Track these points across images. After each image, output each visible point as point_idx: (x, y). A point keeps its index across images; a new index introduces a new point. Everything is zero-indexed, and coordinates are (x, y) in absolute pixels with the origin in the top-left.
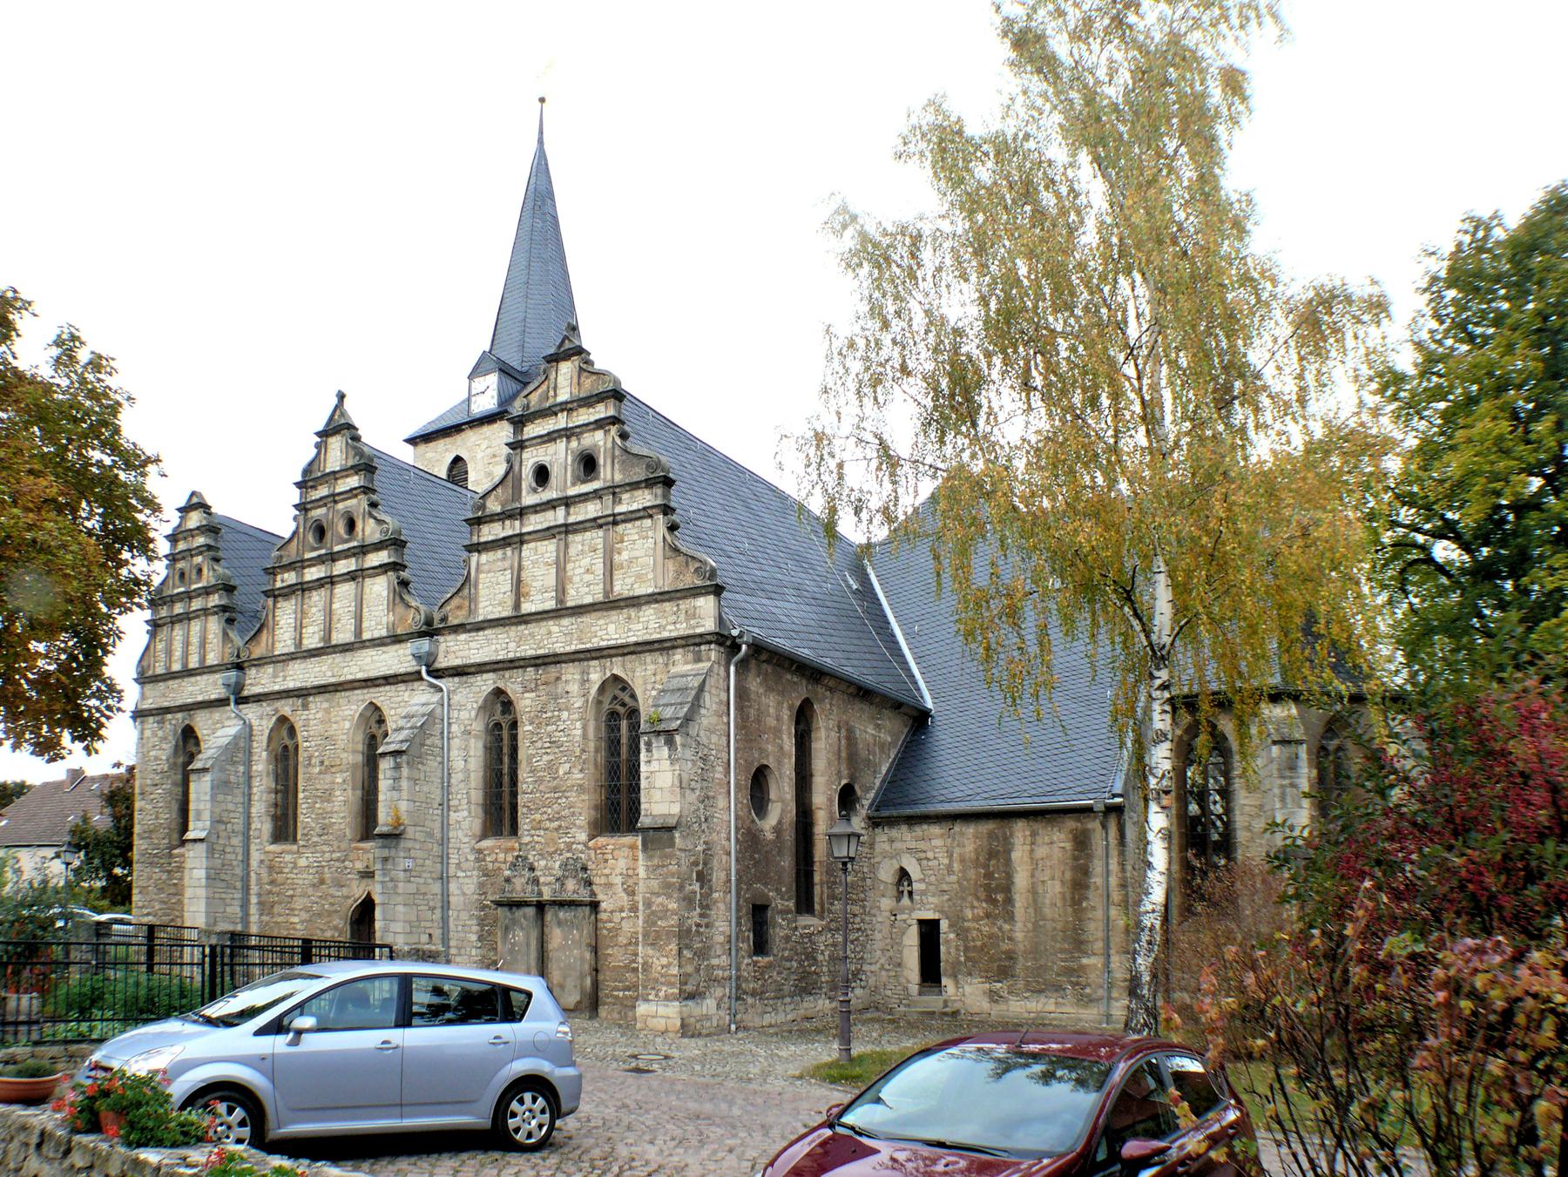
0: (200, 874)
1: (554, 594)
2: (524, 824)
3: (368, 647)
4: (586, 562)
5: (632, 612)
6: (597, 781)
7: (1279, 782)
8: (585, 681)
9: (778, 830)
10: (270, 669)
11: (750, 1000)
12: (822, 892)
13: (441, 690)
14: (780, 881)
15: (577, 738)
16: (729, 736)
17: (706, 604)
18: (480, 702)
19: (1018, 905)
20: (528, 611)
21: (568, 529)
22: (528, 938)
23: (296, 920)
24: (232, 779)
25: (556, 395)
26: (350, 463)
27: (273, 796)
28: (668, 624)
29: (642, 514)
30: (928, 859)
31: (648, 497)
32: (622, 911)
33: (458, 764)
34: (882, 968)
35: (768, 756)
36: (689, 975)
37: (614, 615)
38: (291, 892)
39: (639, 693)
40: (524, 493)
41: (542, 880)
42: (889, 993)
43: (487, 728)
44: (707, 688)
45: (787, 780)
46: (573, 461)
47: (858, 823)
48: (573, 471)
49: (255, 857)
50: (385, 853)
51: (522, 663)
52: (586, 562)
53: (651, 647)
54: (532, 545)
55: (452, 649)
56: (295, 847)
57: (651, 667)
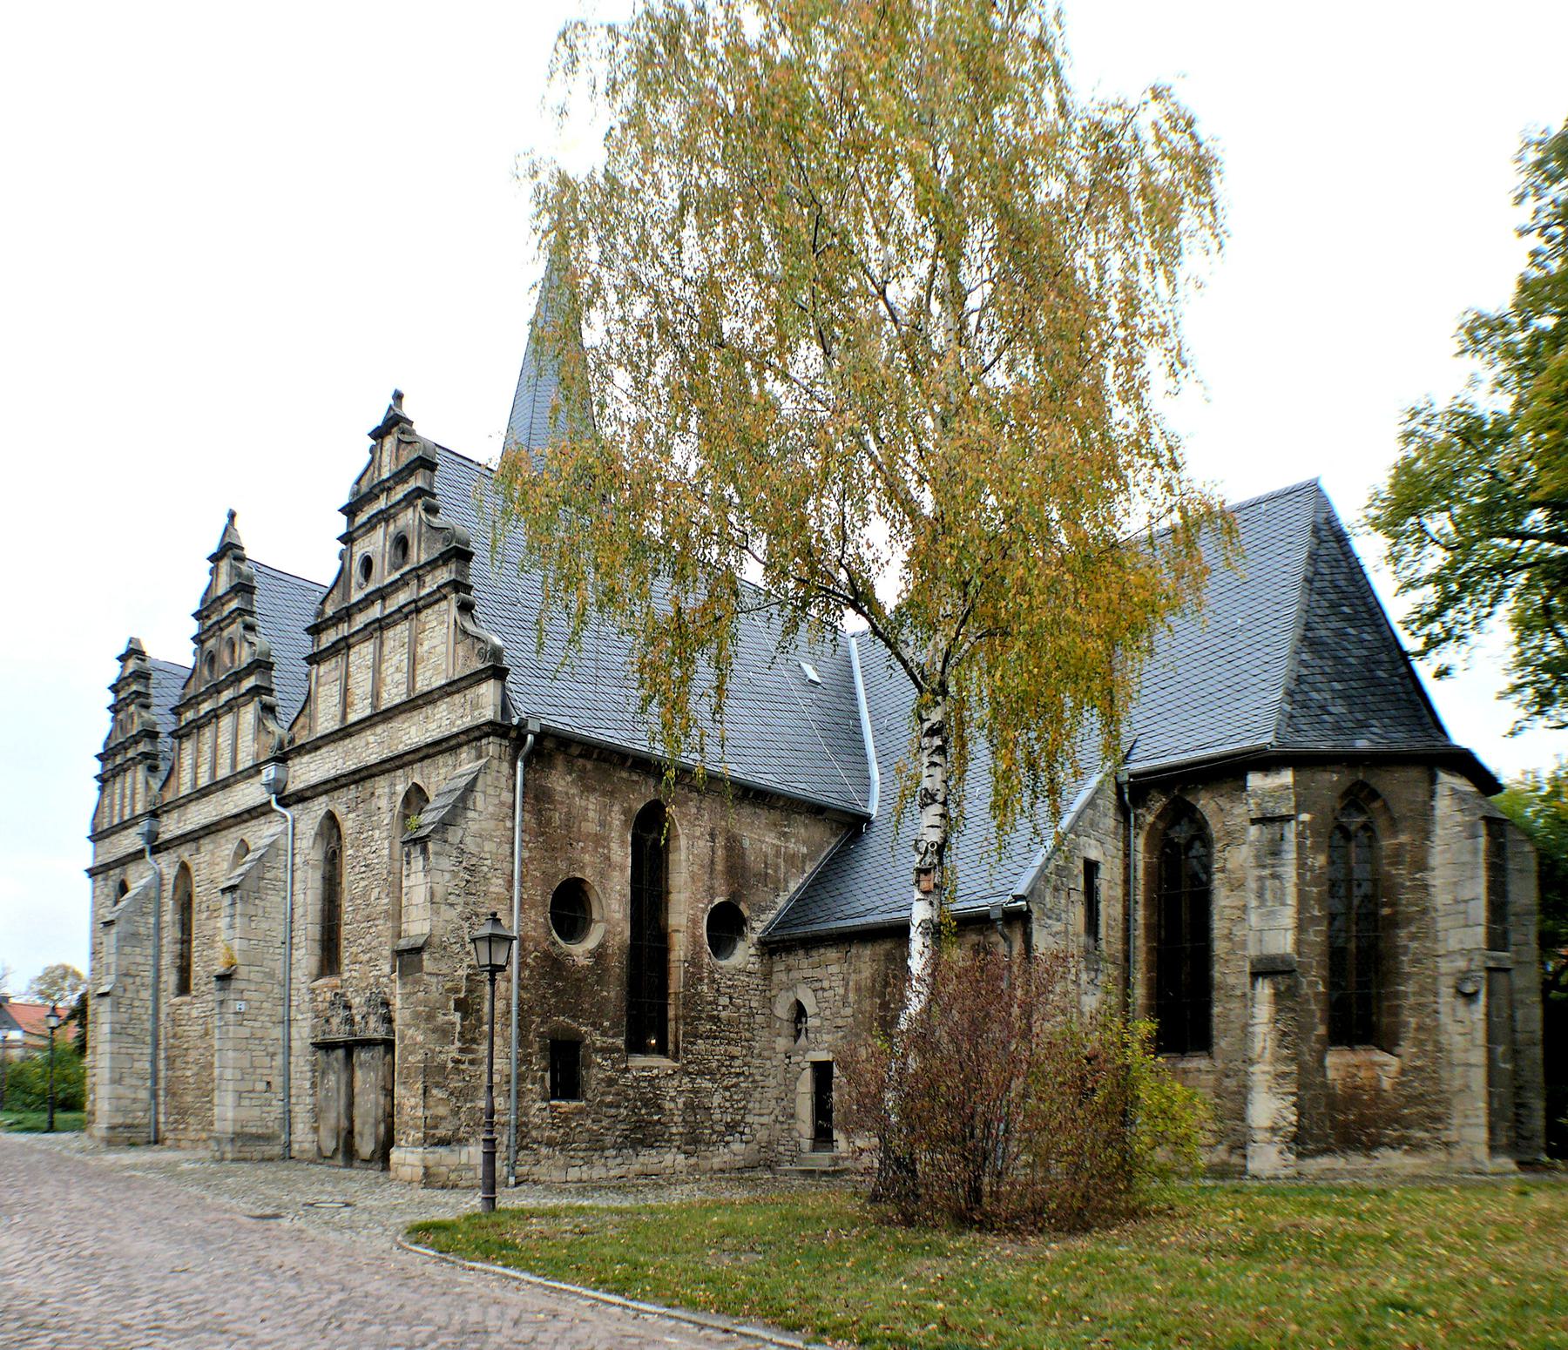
0: (106, 1028)
5: (429, 710)
7: (1257, 872)
9: (599, 954)
10: (175, 815)
11: (544, 1151)
12: (677, 1029)
14: (601, 1013)
17: (488, 691)
22: (338, 1082)
23: (189, 1073)
24: (142, 930)
30: (823, 989)
33: (299, 898)
34: (776, 1121)
35: (582, 868)
36: (442, 1118)
42: (781, 1149)
44: (480, 785)
47: (743, 955)
49: (164, 1009)
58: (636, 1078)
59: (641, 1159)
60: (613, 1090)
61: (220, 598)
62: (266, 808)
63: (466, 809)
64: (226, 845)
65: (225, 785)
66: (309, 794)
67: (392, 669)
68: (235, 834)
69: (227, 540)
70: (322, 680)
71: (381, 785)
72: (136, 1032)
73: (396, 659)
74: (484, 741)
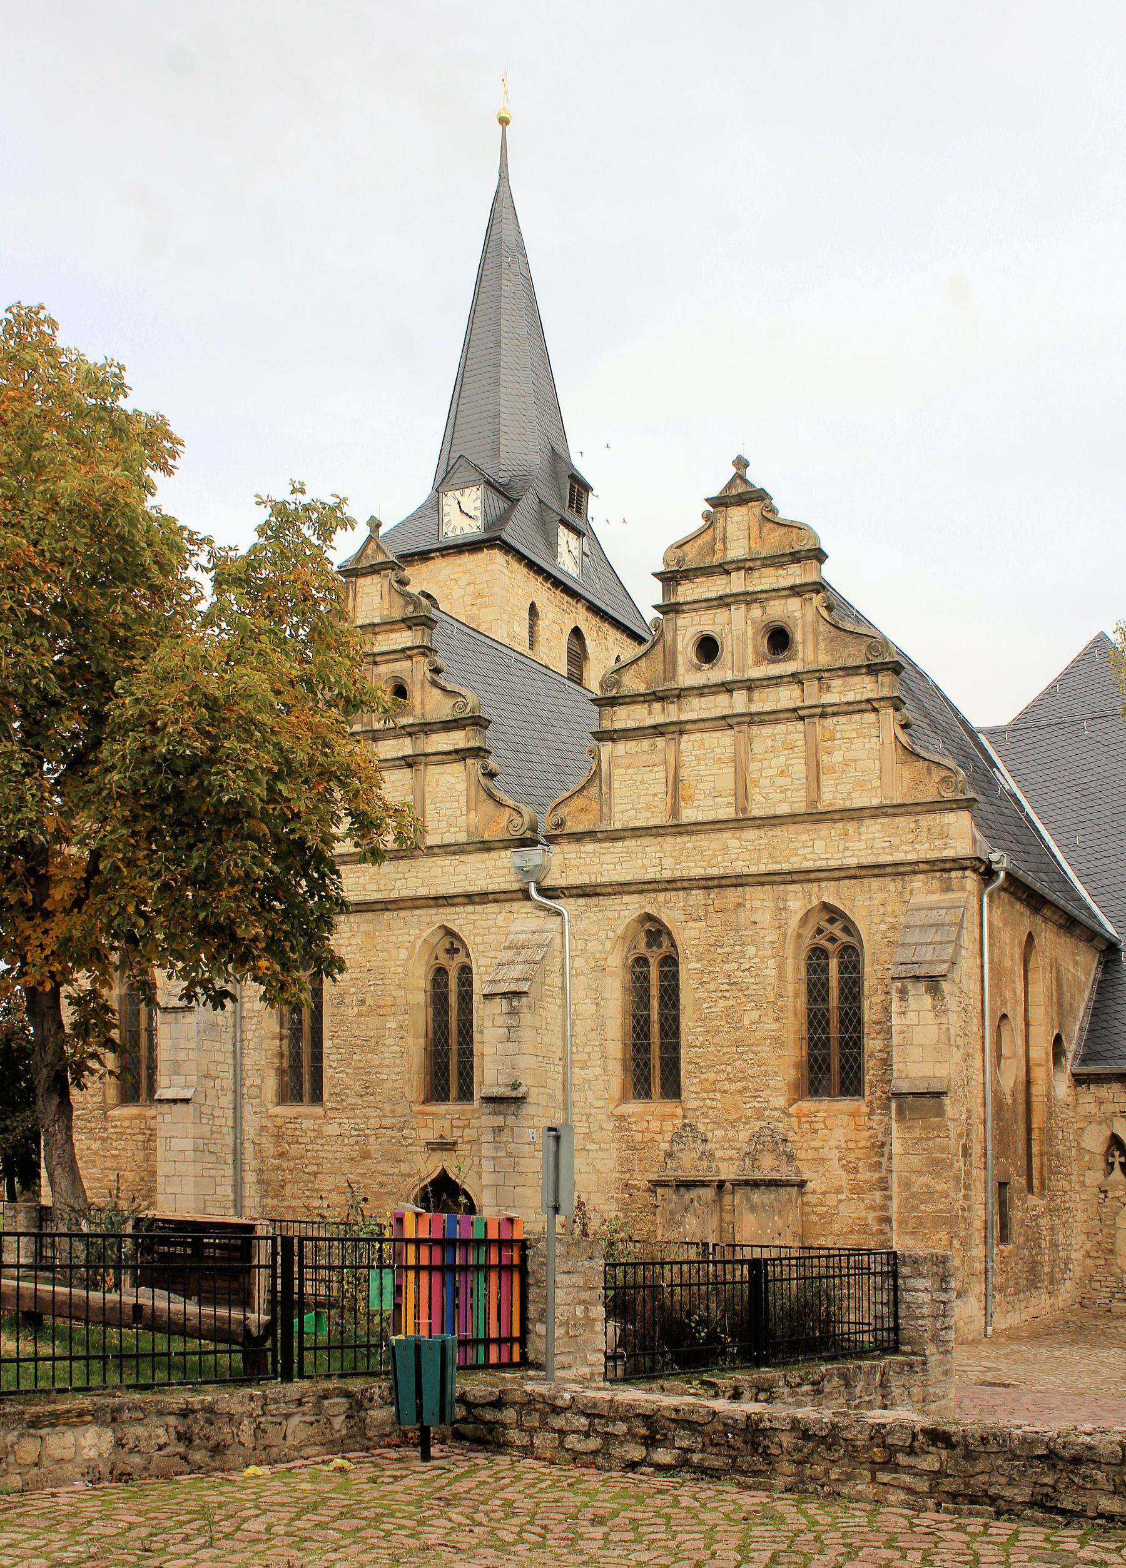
1: (732, 799)
2: (689, 1083)
3: (436, 855)
4: (779, 761)
5: (851, 827)
6: (796, 1032)
8: (780, 909)
13: (559, 914)
15: (771, 980)
16: (982, 981)
18: (620, 931)
20: (693, 820)
21: (753, 719)
25: (725, 549)
26: (397, 615)
27: (278, 1042)
28: (902, 843)
29: (863, 706)
31: (872, 686)
32: (838, 1191)
37: (823, 829)
38: (315, 1168)
39: (861, 925)
40: (681, 670)
41: (718, 1154)
43: (625, 964)
45: (1019, 1032)
46: (755, 634)
48: (755, 647)
50: (499, 1121)
51: (686, 884)
52: (779, 761)
53: (881, 871)
54: (697, 736)
55: (573, 862)
56: (318, 1110)
57: (879, 896)
71: (617, 902)
72: (217, 1149)
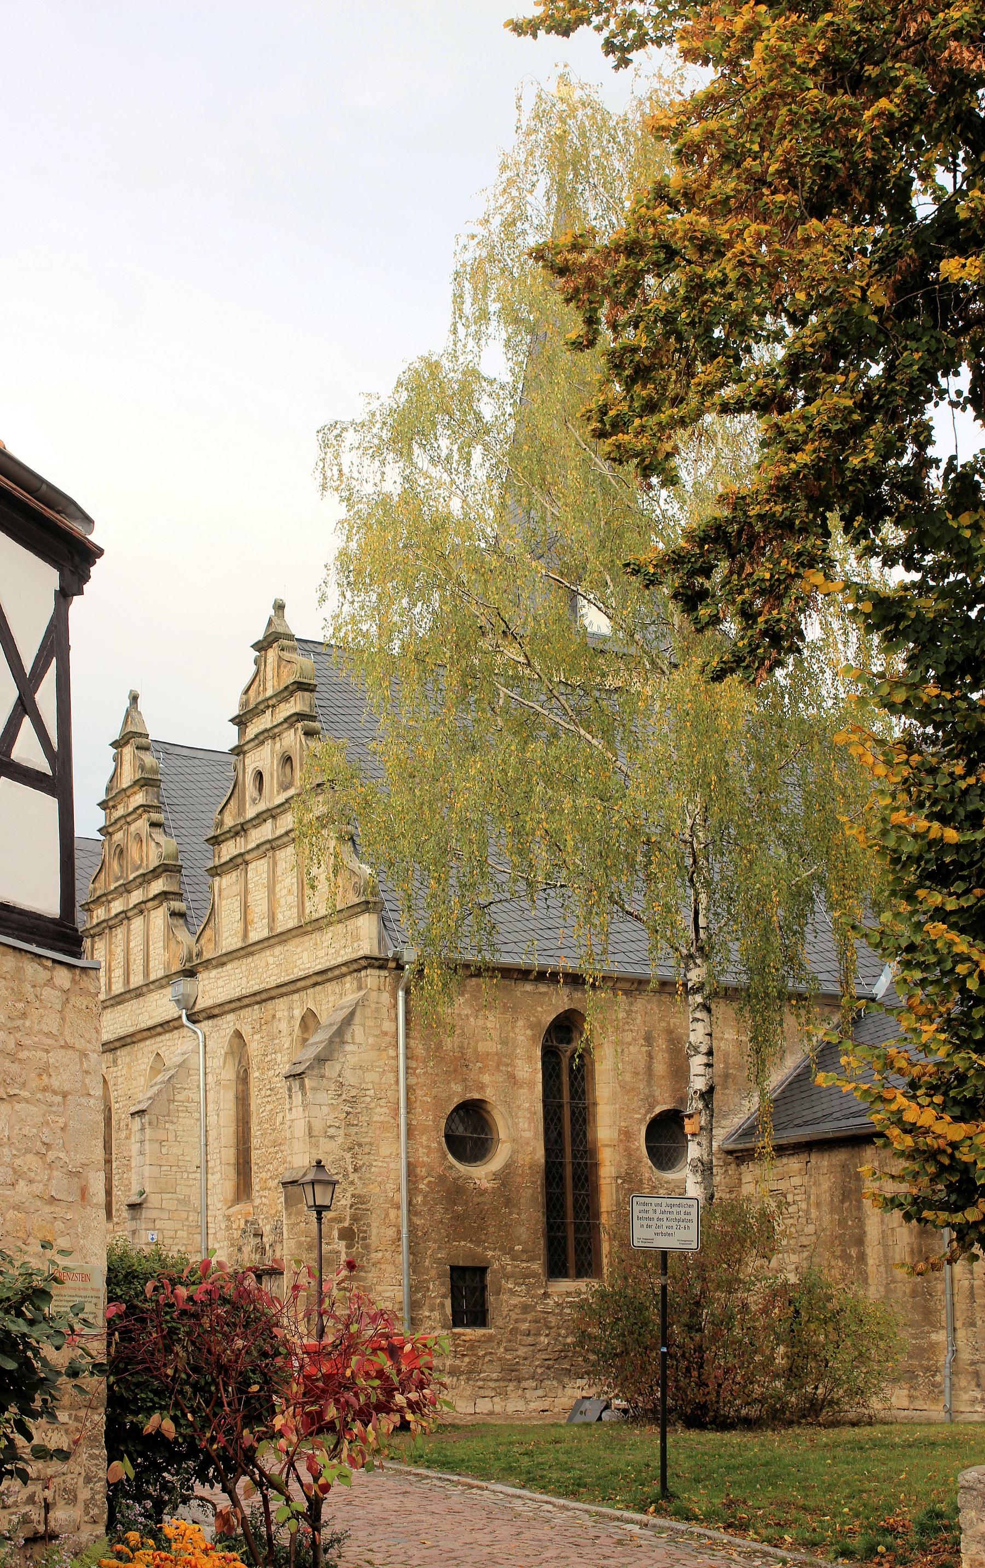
5: (316, 936)
9: (504, 1177)
17: (367, 924)
19: (870, 1262)
33: (212, 1119)
44: (357, 1018)
58: (558, 1305)
59: (569, 1392)
60: (529, 1317)
61: (124, 790)
62: (176, 1024)
63: (343, 1043)
64: (144, 1053)
65: (137, 993)
66: (216, 1011)
67: (285, 892)
68: (150, 1046)
69: (131, 728)
70: (224, 894)
71: (280, 1005)
73: (288, 882)
74: (363, 973)
